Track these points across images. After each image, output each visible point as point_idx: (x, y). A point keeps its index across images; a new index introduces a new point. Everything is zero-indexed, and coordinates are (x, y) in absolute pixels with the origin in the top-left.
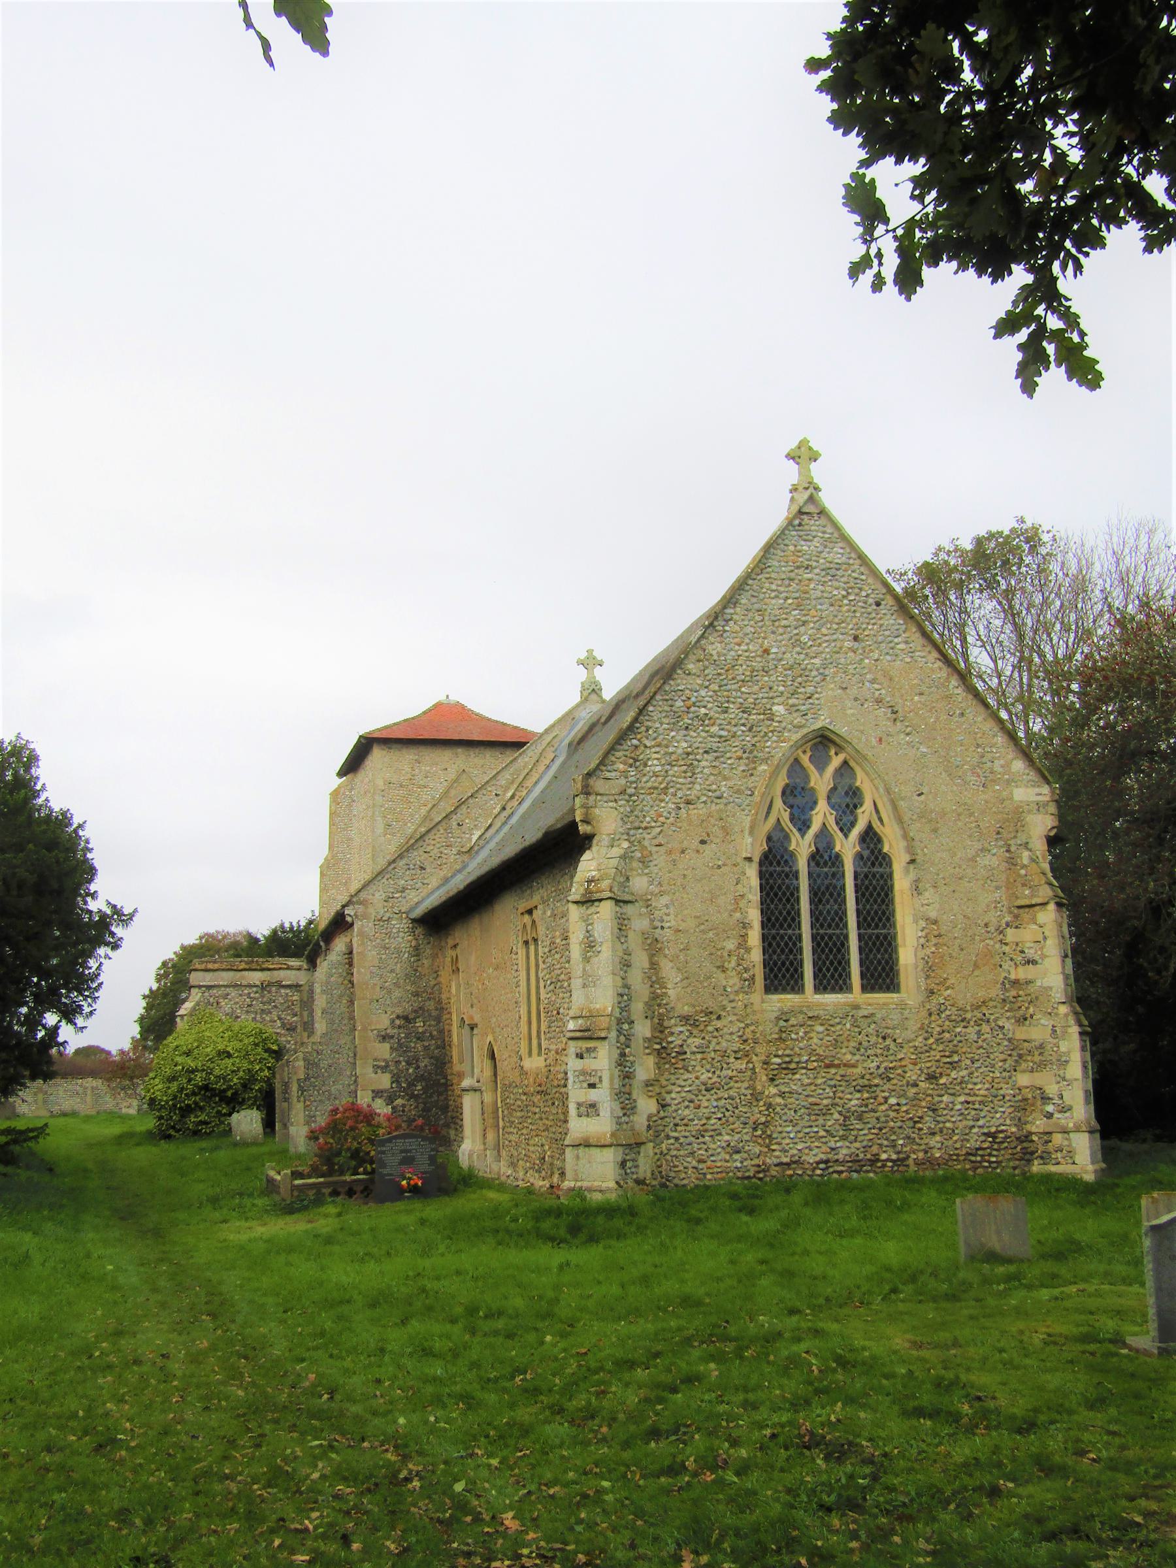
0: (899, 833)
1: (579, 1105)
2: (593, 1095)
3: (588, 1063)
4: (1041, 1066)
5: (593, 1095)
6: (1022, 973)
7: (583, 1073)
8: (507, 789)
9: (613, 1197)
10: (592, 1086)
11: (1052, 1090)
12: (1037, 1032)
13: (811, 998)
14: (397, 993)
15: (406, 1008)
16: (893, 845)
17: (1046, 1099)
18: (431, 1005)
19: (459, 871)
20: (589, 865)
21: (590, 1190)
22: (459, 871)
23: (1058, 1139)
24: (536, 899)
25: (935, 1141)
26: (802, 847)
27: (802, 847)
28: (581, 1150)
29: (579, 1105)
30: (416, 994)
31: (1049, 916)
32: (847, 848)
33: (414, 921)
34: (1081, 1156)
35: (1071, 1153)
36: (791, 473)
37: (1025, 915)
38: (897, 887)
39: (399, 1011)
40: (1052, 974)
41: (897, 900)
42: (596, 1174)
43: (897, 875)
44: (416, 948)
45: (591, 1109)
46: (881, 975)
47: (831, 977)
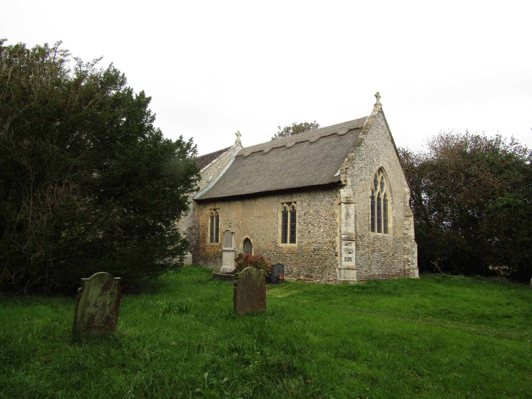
0: (390, 195)
1: (345, 258)
2: (350, 255)
3: (349, 247)
4: (408, 254)
5: (350, 255)
6: (405, 232)
7: (347, 249)
8: (219, 166)
9: (357, 283)
10: (350, 253)
11: (410, 259)
12: (407, 246)
13: (376, 233)
14: (189, 221)
15: (191, 225)
16: (389, 198)
17: (409, 261)
18: (197, 225)
19: (206, 187)
20: (344, 193)
21: (350, 281)
22: (206, 187)
23: (411, 271)
24: (294, 200)
25: (393, 270)
26: (376, 195)
27: (376, 195)
28: (346, 271)
29: (345, 258)
30: (193, 222)
31: (412, 219)
32: (382, 196)
33: (194, 200)
34: (416, 274)
35: (414, 274)
36: (374, 100)
37: (407, 218)
38: (389, 208)
39: (189, 226)
40: (412, 233)
41: (389, 211)
42: (352, 277)
43: (389, 205)
44: (194, 208)
45: (350, 259)
46: (386, 231)
47: (379, 231)
